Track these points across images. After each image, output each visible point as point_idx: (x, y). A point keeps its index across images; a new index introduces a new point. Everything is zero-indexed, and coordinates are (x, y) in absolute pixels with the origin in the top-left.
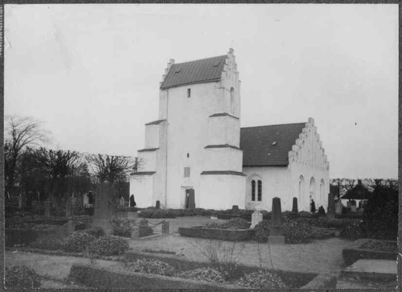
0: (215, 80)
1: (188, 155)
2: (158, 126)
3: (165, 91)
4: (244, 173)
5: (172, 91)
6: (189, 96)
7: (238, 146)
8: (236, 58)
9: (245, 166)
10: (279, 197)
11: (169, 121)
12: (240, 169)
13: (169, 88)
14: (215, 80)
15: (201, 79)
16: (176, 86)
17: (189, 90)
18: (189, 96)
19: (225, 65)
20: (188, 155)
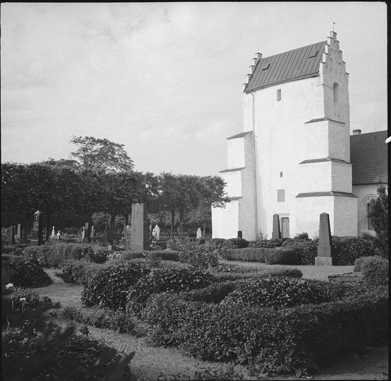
0: (312, 75)
1: (281, 175)
2: (243, 139)
3: (250, 95)
4: (354, 194)
5: (259, 93)
6: (279, 99)
7: (349, 162)
8: (340, 43)
9: (355, 184)
10: (305, 232)
11: (256, 133)
12: (349, 189)
13: (253, 90)
14: (312, 75)
15: (279, 80)
16: (263, 88)
17: (279, 91)
18: (279, 99)
19: (251, 73)
20: (281, 175)
